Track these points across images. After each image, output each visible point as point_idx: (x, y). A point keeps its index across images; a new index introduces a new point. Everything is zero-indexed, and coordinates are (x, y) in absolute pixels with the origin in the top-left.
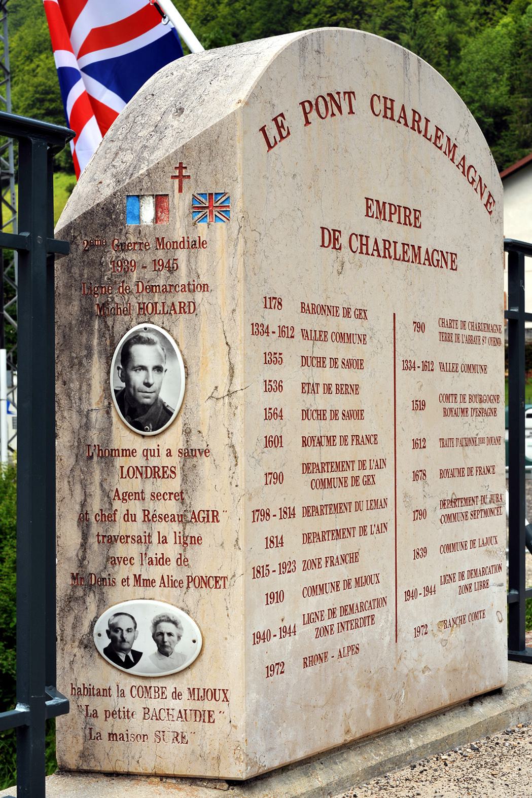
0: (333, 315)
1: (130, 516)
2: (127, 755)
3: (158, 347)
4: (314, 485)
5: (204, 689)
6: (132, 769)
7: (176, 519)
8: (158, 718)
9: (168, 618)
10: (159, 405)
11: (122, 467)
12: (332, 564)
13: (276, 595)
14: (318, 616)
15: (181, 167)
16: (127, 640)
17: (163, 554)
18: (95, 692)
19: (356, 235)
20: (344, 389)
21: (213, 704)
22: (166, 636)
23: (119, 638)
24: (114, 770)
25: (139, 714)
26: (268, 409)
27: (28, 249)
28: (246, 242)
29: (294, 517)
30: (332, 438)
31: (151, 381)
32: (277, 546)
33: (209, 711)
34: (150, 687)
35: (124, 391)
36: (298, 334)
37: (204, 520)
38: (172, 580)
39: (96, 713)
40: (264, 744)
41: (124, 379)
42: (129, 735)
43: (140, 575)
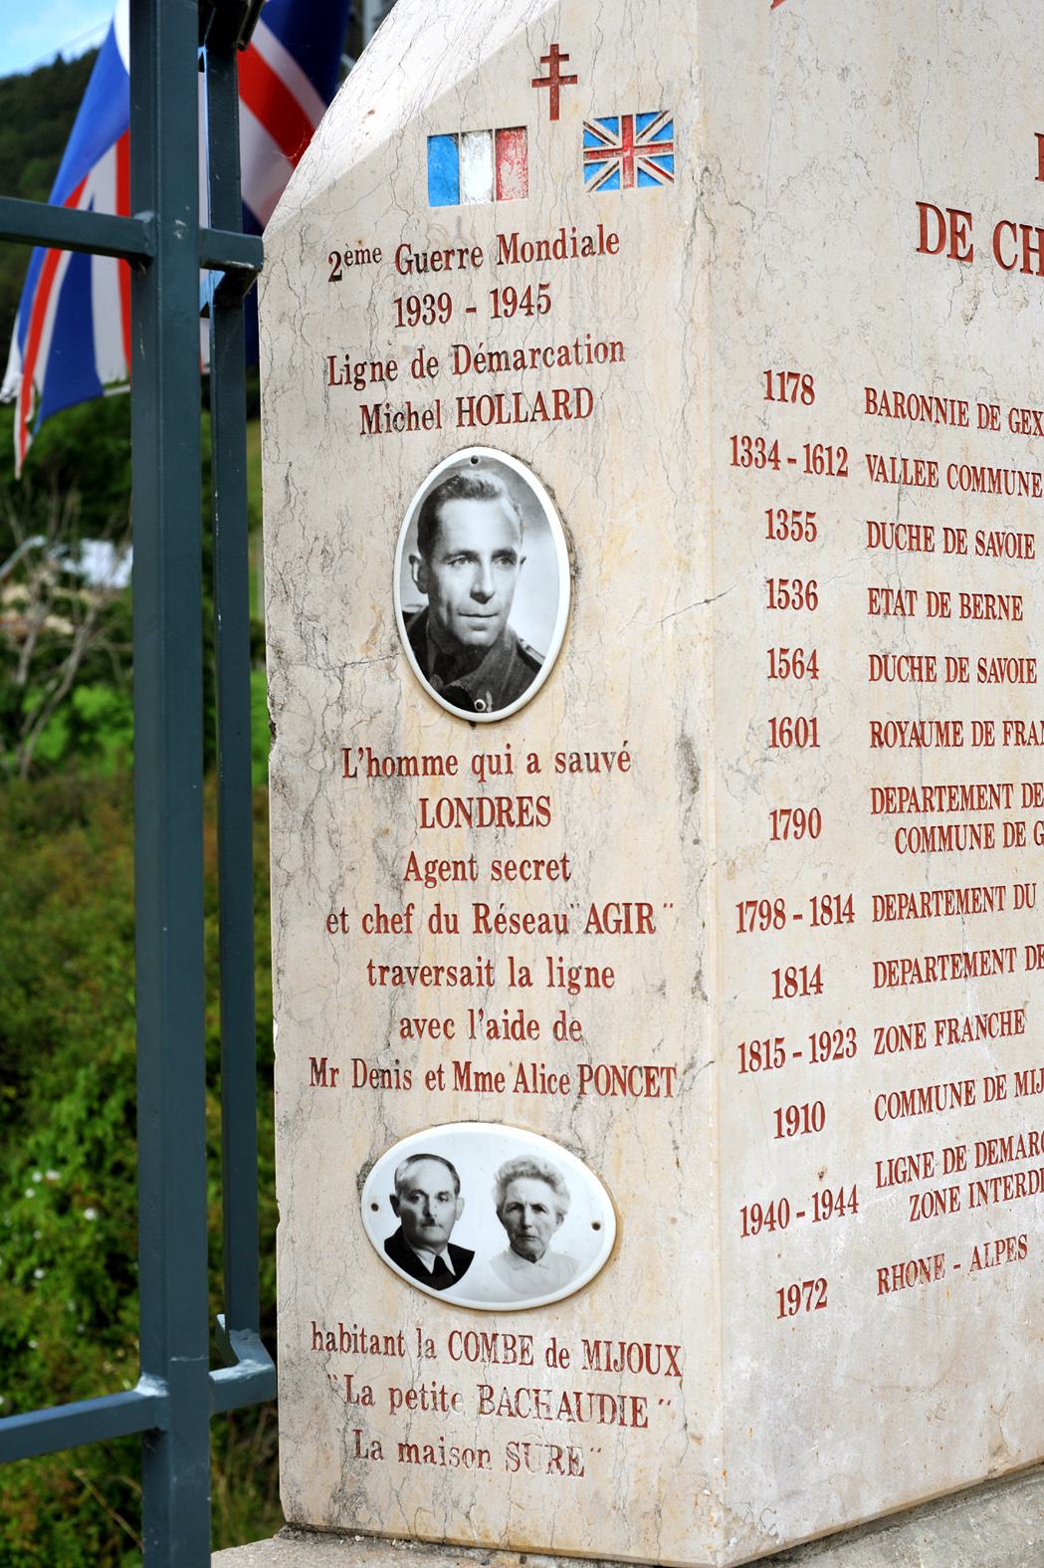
0: (953, 423)
1: (443, 919)
2: (441, 1498)
3: (505, 502)
4: (903, 841)
5: (622, 1344)
6: (453, 1534)
7: (552, 926)
8: (514, 1411)
9: (534, 1167)
10: (508, 645)
11: (424, 801)
12: (954, 1038)
13: (802, 1113)
14: (918, 1166)
15: (555, 56)
16: (436, 1221)
17: (521, 1011)
18: (368, 1344)
19: (1013, 226)
20: (983, 607)
21: (643, 1380)
22: (528, 1211)
23: (420, 1216)
24: (413, 1532)
25: (469, 1400)
26: (777, 653)
27: (150, 253)
28: (714, 232)
29: (851, 921)
30: (951, 726)
31: (488, 589)
32: (805, 993)
33: (635, 1399)
34: (495, 1336)
35: (425, 614)
36: (858, 469)
37: (618, 929)
38: (543, 1075)
39: (370, 1395)
40: (773, 1482)
41: (424, 586)
42: (447, 1450)
43: (468, 1064)
